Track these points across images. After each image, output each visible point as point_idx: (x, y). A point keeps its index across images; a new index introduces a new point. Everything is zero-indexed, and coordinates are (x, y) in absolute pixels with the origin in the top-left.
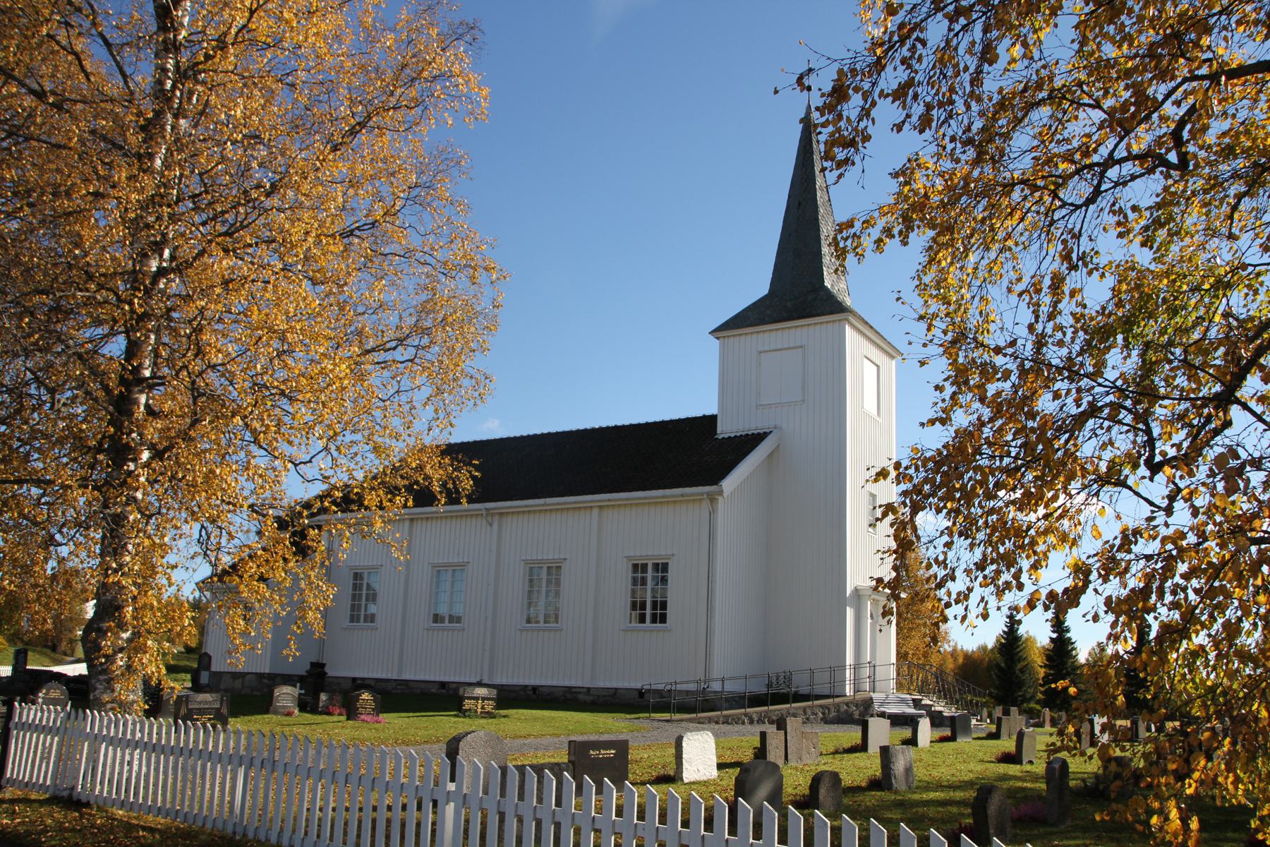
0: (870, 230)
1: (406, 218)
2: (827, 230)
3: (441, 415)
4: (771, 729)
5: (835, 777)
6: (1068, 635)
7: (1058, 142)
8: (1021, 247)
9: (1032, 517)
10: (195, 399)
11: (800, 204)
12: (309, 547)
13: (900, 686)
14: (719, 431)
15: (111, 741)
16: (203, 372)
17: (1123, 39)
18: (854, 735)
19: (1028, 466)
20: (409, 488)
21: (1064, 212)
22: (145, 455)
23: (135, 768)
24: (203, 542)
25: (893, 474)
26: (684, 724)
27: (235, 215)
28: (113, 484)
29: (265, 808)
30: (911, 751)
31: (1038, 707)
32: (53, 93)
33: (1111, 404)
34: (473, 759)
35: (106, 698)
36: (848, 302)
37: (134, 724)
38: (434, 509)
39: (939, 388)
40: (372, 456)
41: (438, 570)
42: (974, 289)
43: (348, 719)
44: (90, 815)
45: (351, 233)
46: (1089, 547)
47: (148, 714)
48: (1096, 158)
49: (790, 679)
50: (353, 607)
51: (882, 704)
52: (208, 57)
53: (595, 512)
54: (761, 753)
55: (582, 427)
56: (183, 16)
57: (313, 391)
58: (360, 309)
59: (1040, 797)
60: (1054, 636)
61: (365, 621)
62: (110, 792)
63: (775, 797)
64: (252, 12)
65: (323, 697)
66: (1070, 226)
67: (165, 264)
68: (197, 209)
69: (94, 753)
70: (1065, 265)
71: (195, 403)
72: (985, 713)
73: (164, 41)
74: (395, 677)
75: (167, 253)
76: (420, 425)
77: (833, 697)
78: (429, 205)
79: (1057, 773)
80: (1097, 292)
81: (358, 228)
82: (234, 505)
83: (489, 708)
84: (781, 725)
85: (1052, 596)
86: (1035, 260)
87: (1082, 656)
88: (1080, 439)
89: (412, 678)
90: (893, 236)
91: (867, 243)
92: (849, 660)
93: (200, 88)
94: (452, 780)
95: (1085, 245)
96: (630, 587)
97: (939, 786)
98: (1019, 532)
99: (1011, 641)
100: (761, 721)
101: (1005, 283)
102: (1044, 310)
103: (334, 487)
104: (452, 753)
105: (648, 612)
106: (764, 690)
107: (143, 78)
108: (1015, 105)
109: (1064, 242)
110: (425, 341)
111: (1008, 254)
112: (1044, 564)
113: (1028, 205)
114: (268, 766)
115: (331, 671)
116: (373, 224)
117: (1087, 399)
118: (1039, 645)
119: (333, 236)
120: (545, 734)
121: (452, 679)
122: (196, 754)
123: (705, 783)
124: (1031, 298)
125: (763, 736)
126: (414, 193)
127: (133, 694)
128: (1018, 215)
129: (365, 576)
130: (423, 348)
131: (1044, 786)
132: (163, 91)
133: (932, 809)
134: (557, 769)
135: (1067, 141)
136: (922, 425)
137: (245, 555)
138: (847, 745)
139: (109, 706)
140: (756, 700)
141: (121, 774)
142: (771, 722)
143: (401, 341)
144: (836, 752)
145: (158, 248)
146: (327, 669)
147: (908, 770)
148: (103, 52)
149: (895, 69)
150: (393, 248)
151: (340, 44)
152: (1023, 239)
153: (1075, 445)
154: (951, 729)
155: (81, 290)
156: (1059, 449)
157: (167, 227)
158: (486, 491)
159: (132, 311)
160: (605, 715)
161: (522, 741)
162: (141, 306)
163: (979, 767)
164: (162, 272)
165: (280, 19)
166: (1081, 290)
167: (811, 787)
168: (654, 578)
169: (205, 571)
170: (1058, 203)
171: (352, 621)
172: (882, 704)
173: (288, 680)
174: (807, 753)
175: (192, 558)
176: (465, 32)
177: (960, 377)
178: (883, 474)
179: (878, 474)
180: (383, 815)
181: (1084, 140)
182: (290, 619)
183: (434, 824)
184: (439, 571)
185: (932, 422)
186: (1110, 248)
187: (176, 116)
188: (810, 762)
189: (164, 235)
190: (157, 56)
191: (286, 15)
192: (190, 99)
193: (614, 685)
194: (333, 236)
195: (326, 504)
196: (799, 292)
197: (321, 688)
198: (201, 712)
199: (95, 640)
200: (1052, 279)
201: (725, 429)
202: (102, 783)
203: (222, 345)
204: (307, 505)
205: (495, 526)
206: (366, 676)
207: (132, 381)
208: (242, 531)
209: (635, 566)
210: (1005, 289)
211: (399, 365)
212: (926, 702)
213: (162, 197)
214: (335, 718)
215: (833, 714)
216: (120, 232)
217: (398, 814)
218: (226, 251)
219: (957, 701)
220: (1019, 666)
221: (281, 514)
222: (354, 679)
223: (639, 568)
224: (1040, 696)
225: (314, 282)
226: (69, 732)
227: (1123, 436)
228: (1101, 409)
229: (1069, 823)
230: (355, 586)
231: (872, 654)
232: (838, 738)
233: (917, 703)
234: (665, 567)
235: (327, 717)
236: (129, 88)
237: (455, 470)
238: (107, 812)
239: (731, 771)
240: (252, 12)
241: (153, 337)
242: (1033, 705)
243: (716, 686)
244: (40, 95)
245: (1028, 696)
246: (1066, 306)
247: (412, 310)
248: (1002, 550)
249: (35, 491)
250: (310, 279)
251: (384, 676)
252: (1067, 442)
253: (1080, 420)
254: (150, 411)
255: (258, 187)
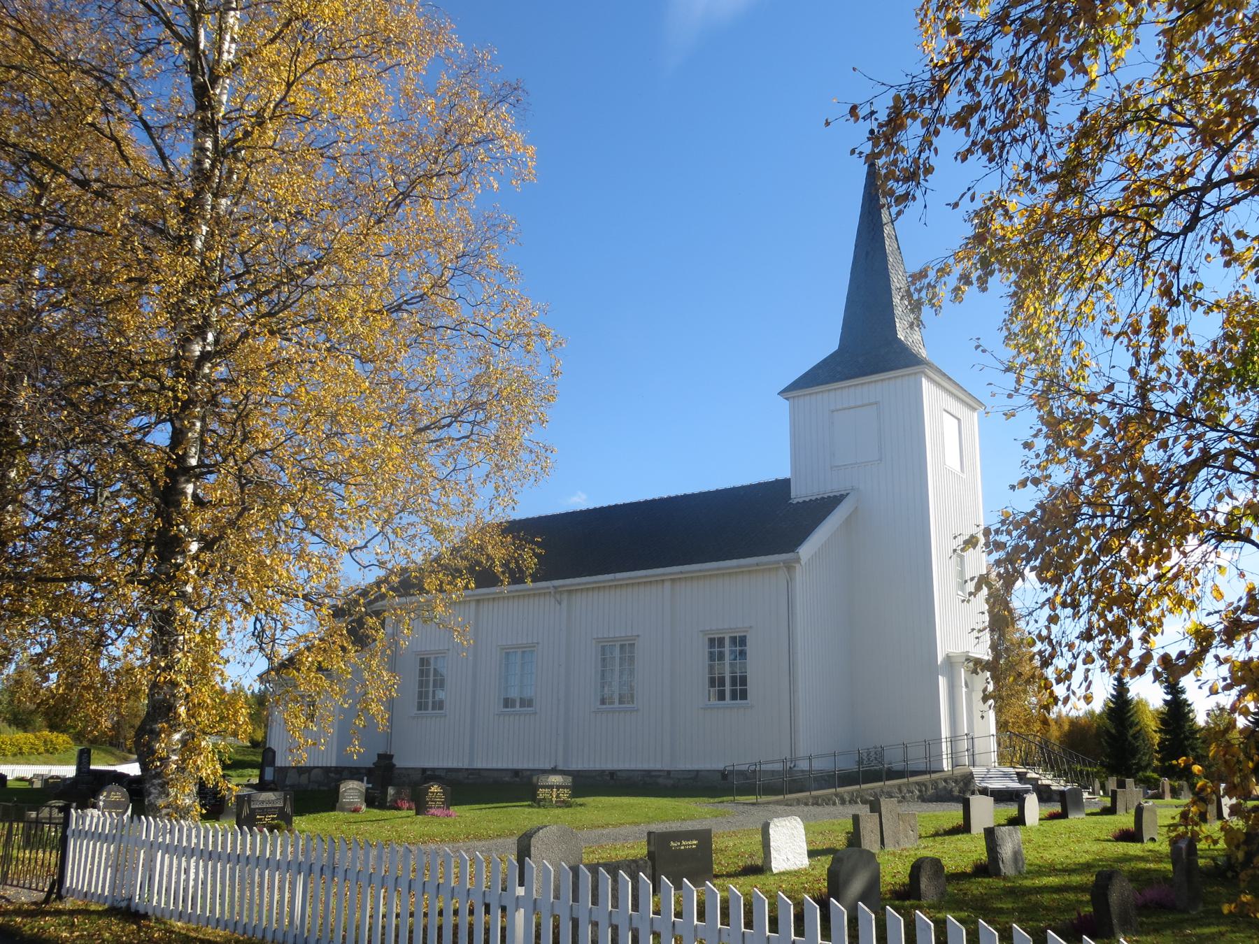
0: (946, 278)
1: (453, 290)
2: (898, 281)
3: (502, 492)
4: (863, 810)
5: (936, 864)
6: (1184, 696)
7: (1148, 167)
8: (1114, 284)
9: (1142, 579)
10: (242, 486)
11: (867, 253)
12: (368, 637)
13: (1001, 758)
14: (793, 495)
15: (167, 849)
16: (252, 457)
17: (1214, 52)
18: (953, 814)
19: (1134, 525)
20: (471, 570)
21: (1159, 243)
22: (194, 547)
23: (192, 876)
24: (259, 635)
25: (982, 540)
26: (771, 807)
27: (279, 293)
28: (162, 581)
29: (325, 918)
30: (1019, 833)
31: (1155, 776)
32: (97, 180)
33: (1225, 451)
34: (544, 863)
35: (161, 802)
36: (924, 353)
37: (190, 830)
38: (496, 589)
39: (1028, 446)
40: (431, 538)
41: (507, 653)
42: (1064, 334)
43: (417, 814)
44: (148, 927)
45: (399, 308)
46: (1209, 615)
47: (204, 817)
48: (1191, 182)
49: (882, 756)
50: (420, 695)
51: (983, 779)
52: (247, 134)
53: (668, 585)
54: (854, 839)
55: (649, 497)
56: (221, 94)
57: (366, 474)
58: (412, 387)
59: (1166, 879)
60: (1169, 697)
61: (433, 709)
62: (167, 903)
63: (872, 895)
64: (289, 85)
65: (391, 791)
66: (1167, 258)
67: (209, 348)
68: (240, 290)
69: (150, 861)
70: (1166, 300)
71: (242, 491)
72: (1097, 784)
73: (202, 120)
74: (466, 766)
75: (210, 337)
76: (480, 503)
77: (930, 772)
78: (478, 273)
79: (1184, 850)
80: (1205, 329)
81: (406, 302)
82: (287, 595)
83: (564, 797)
84: (875, 807)
85: (1165, 659)
86: (1133, 298)
87: (1201, 720)
88: (1193, 491)
89: (484, 766)
90: (971, 283)
91: (944, 292)
92: (945, 732)
93: (239, 166)
94: (521, 884)
95: (1186, 278)
96: (707, 662)
97: (1053, 870)
98: (1128, 597)
99: (1121, 705)
100: (853, 801)
101: (1099, 324)
102: (1146, 351)
103: (392, 571)
104: (524, 851)
105: (728, 688)
106: (855, 768)
107: (182, 159)
108: (1096, 133)
109: (1163, 276)
110: (481, 416)
111: (1100, 293)
112: (1159, 630)
113: (1118, 238)
114: (328, 873)
115: (399, 762)
116: (421, 296)
117: (1197, 447)
118: (1151, 708)
119: (380, 312)
120: (623, 826)
121: (525, 767)
122: (253, 861)
123: (796, 874)
124: (1130, 340)
125: (856, 819)
126: (461, 263)
127: (186, 797)
128: (1107, 252)
129: (432, 661)
130: (479, 424)
131: (1170, 867)
132: (201, 170)
133: (1046, 896)
134: (633, 867)
135: (1160, 166)
136: (1013, 487)
137: (302, 646)
138: (948, 826)
139: (164, 811)
140: (848, 779)
141: (178, 883)
142: (864, 802)
143: (456, 417)
144: (936, 834)
145: (200, 332)
146: (395, 761)
147: (1017, 855)
148: (144, 135)
149: (960, 93)
150: (445, 321)
151: (380, 112)
152: (1115, 275)
153: (1187, 498)
154: (1063, 804)
155: (122, 379)
156: (1169, 504)
157: (209, 310)
158: (551, 569)
159: (176, 398)
160: (687, 800)
161: (600, 831)
162: (184, 392)
163: (1096, 847)
164: (205, 357)
165: (319, 90)
166: (1185, 327)
167: (911, 876)
168: (732, 652)
169: (262, 665)
170: (1152, 234)
171: (420, 708)
172: (983, 779)
173: (355, 773)
174: (905, 838)
175: (248, 652)
176: (507, 94)
177: (1053, 425)
178: (971, 542)
179: (966, 542)
180: (449, 920)
181: (1178, 162)
182: (352, 713)
183: (503, 929)
184: (507, 654)
185: (1023, 484)
186: (1219, 281)
187: (215, 195)
188: (908, 846)
189: (206, 318)
190: (195, 135)
191: (324, 86)
192: (229, 178)
193: (696, 767)
194: (380, 312)
195: (383, 590)
196: (870, 347)
197: (389, 783)
198: (264, 811)
199: (149, 742)
200: (1152, 318)
201: (799, 493)
202: (159, 893)
203: (270, 428)
204: (364, 593)
205: (564, 604)
206: (435, 765)
207: (179, 470)
208: (299, 625)
209: (712, 641)
210: (1098, 331)
211: (455, 442)
212: (1031, 775)
213: (203, 279)
214: (404, 813)
215: (931, 792)
216: (163, 318)
217: (465, 920)
218: (272, 333)
219: (1066, 774)
220: (1131, 732)
221: (339, 604)
222: (424, 770)
223: (715, 642)
224: (1156, 763)
225: (363, 360)
226: (124, 839)
227: (1241, 486)
228: (1216, 456)
229: (1201, 908)
230: (421, 672)
231: (970, 731)
232: (937, 818)
233: (1021, 777)
234: (743, 641)
235: (396, 812)
236: (168, 169)
237: (517, 548)
238: (165, 923)
239: (823, 858)
240: (289, 85)
241: (198, 424)
242: (1149, 773)
243: (803, 765)
244: (84, 184)
245: (1143, 764)
246: (1171, 345)
247: (466, 385)
248: (1110, 617)
249: (86, 587)
250: (359, 358)
251: (455, 765)
252: (1178, 494)
253: (1192, 470)
254: (199, 502)
255: (302, 264)
